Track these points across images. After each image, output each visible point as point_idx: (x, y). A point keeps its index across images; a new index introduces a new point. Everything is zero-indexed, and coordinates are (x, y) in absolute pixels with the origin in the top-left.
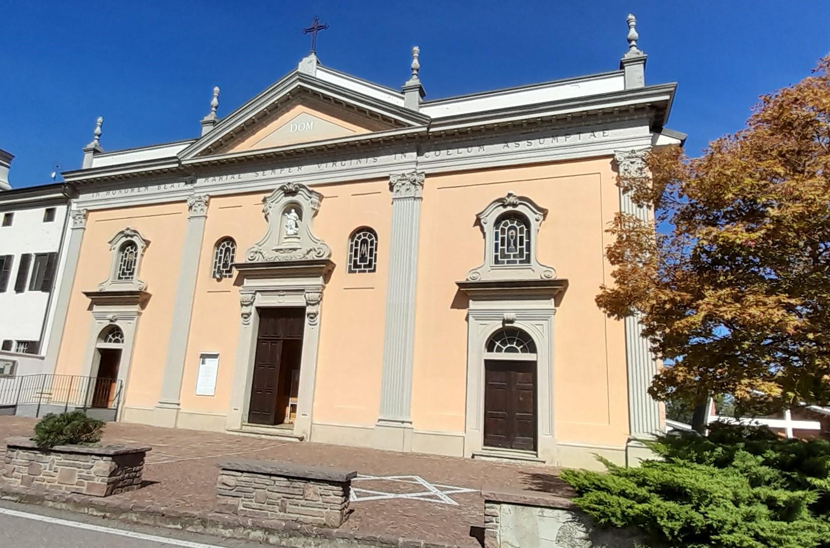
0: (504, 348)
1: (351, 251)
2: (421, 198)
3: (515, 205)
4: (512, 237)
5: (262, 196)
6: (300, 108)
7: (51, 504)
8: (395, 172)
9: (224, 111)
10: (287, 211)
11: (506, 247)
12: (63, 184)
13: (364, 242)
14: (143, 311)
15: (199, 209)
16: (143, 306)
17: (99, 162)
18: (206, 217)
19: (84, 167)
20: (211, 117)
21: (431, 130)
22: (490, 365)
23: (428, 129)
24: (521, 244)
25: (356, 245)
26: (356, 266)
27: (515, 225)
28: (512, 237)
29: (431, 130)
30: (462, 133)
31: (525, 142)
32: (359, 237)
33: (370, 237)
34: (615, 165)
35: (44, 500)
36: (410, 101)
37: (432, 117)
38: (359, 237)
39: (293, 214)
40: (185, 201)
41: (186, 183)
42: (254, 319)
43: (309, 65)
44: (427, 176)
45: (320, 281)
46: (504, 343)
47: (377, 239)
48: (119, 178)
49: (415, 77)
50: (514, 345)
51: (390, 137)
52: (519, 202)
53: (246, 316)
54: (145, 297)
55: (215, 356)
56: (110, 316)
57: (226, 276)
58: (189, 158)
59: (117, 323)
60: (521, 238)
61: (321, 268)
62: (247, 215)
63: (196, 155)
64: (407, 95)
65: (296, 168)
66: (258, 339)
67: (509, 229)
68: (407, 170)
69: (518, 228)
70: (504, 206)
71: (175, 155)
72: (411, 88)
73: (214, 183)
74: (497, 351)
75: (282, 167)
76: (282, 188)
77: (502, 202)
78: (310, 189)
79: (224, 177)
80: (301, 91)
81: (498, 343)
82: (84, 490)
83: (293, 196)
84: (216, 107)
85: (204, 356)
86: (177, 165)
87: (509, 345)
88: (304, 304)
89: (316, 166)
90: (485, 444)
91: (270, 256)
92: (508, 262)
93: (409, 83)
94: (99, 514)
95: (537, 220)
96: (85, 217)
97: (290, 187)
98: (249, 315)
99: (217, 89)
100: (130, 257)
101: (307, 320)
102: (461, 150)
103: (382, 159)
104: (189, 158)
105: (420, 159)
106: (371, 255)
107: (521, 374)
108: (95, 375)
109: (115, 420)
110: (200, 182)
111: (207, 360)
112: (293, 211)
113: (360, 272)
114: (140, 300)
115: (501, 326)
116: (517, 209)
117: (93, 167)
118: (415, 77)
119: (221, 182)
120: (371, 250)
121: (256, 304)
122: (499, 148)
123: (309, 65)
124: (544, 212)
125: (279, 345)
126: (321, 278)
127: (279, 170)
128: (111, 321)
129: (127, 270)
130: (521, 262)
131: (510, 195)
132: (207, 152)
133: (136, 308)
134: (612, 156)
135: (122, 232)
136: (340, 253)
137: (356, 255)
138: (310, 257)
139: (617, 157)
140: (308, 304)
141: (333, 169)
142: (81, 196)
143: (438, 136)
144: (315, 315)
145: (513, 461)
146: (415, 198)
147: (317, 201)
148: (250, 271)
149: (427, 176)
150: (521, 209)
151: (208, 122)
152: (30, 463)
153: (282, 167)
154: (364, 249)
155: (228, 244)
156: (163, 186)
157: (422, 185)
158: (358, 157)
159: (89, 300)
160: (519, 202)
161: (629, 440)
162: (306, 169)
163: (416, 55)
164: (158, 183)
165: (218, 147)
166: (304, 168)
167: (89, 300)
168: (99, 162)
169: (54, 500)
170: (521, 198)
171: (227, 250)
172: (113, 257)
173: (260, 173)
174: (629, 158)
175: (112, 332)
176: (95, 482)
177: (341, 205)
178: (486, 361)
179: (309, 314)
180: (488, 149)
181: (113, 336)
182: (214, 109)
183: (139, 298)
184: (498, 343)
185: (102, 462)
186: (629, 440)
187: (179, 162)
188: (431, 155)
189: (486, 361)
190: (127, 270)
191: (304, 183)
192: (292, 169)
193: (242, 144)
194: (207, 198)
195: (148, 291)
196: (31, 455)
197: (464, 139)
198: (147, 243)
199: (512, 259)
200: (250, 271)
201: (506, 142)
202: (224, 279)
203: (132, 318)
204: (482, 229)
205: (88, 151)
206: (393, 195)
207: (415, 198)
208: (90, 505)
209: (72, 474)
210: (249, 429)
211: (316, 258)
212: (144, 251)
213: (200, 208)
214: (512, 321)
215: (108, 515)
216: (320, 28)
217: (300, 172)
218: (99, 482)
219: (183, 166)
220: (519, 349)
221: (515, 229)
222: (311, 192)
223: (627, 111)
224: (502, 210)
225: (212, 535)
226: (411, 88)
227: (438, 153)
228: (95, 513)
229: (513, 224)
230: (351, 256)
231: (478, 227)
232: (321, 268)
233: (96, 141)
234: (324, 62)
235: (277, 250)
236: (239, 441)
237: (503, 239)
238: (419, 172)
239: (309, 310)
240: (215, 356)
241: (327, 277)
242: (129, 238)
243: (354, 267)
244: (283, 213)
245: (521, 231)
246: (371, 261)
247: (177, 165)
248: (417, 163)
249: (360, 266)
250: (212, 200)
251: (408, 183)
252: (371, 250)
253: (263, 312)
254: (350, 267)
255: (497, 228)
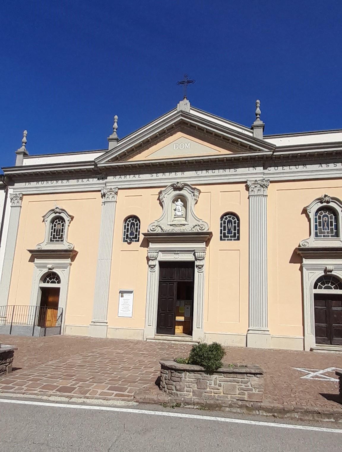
0: (50, 281)
1: (125, 229)
2: (267, 196)
3: (60, 213)
4: (326, 221)
5: (159, 190)
6: (179, 134)
7: (227, 409)
8: (251, 179)
9: (123, 134)
10: (175, 200)
11: (55, 233)
12: (3, 175)
13: (230, 221)
14: (73, 263)
15: (111, 196)
16: (73, 260)
17: (28, 162)
18: (116, 202)
19: (17, 165)
20: (114, 136)
21: (275, 154)
22: (317, 297)
23: (273, 153)
24: (332, 225)
25: (128, 225)
26: (225, 236)
27: (327, 214)
28: (326, 221)
29: (275, 154)
30: (295, 156)
31: (333, 164)
32: (130, 221)
33: (233, 219)
34: (247, 188)
35: (221, 407)
36: (258, 134)
37: (277, 145)
38: (226, 219)
39: (180, 203)
40: (100, 191)
41: (98, 179)
42: (157, 268)
43: (184, 106)
44: (271, 182)
45: (203, 245)
46: (323, 284)
47: (140, 222)
48: (47, 173)
49: (258, 119)
50: (329, 285)
51: (242, 157)
52: (331, 200)
53: (152, 267)
54: (75, 253)
55: (131, 292)
56: (50, 266)
57: (133, 241)
58: (103, 162)
59: (54, 270)
60: (331, 222)
61: (204, 237)
62: (145, 201)
63: (108, 161)
64: (255, 130)
65: (180, 173)
66: (159, 281)
67: (323, 216)
68: (259, 178)
69: (329, 216)
70: (322, 202)
71: (93, 160)
72: (257, 126)
73: (120, 180)
74: (319, 288)
75: (63, 179)
76: (172, 186)
77: (321, 200)
78: (193, 187)
79: (128, 176)
80: (182, 122)
81: (48, 279)
82: (246, 397)
83: (180, 190)
84: (117, 129)
85: (122, 293)
86: (93, 167)
87: (326, 285)
88: (194, 259)
89: (194, 172)
90: (316, 343)
91: (168, 229)
92: (324, 236)
93: (256, 123)
94: (268, 414)
95: (68, 221)
96: (21, 199)
97: (179, 185)
98: (155, 266)
99: (116, 117)
100: (59, 227)
101: (196, 269)
102: (291, 167)
103: (240, 170)
104: (103, 162)
105: (266, 171)
106: (136, 232)
107: (334, 301)
108: (39, 305)
109: (60, 334)
110: (110, 179)
111: (125, 295)
112: (179, 200)
113: (228, 240)
114: (71, 256)
115: (323, 274)
116: (61, 215)
117: (24, 165)
118: (258, 119)
119: (125, 179)
120: (137, 229)
121: (159, 259)
122: (316, 167)
123: (184, 106)
124: (72, 218)
125: (175, 285)
126: (205, 243)
127: (168, 174)
128: (50, 269)
129: (57, 235)
130: (332, 236)
131: (326, 196)
132: (116, 159)
133: (68, 261)
134: (246, 182)
135: (53, 210)
136: (214, 227)
137: (225, 230)
138: (195, 231)
139: (249, 183)
140: (196, 259)
141: (56, 185)
142: (15, 184)
143: (279, 157)
144: (202, 266)
145: (337, 352)
146: (264, 196)
147: (198, 194)
148: (150, 239)
149: (271, 182)
150: (332, 204)
151: (112, 140)
152: (198, 381)
153: (170, 172)
154: (230, 226)
155: (59, 221)
156: (80, 180)
157: (267, 187)
158: (224, 168)
159: (30, 255)
160: (331, 200)
161: (248, 330)
162: (187, 174)
163: (116, 120)
164: (78, 178)
165: (123, 156)
166: (185, 173)
167: (30, 255)
168: (28, 162)
169: (230, 406)
170: (332, 198)
171: (133, 224)
172: (46, 228)
173: (155, 175)
174: (254, 184)
175: (51, 276)
176: (254, 392)
177: (213, 198)
178: (315, 295)
179: (197, 266)
180: (309, 167)
181: (50, 279)
182: (115, 130)
183: (70, 254)
184: (48, 279)
185: (256, 378)
186: (248, 330)
187: (96, 165)
188: (272, 170)
189: (315, 295)
190: (57, 235)
191: (189, 183)
192: (177, 173)
193: (139, 155)
194: (117, 190)
195: (75, 249)
196: (198, 375)
197: (338, 157)
198: (72, 218)
199: (58, 239)
200: (150, 239)
201: (120, 175)
202: (132, 243)
203: (66, 268)
204: (308, 216)
205: (19, 153)
206: (104, 200)
207: (264, 196)
208: (260, 408)
209: (234, 387)
210: (157, 337)
211: (200, 231)
212: (70, 223)
213: (16, 201)
214: (331, 271)
215: (276, 414)
216: (189, 82)
217: (183, 176)
218: (257, 392)
219: (98, 167)
220: (56, 281)
221: (327, 216)
222: (194, 189)
223: (296, 157)
224: (320, 205)
225: (235, 413)
226: (257, 126)
227: (276, 168)
228: (265, 414)
229: (58, 222)
230: (125, 232)
231: (304, 215)
232: (204, 237)
233: (23, 147)
234: (194, 105)
235: (171, 225)
236: (151, 345)
237: (55, 229)
238: (266, 179)
239: (197, 263)
240: (131, 292)
241: (207, 242)
242: (58, 214)
243: (223, 237)
244: (173, 202)
245: (331, 218)
246: (136, 235)
247: (93, 167)
248: (264, 174)
249: (56, 238)
250: (24, 197)
251: (114, 193)
252: (137, 229)
253: (162, 264)
254: (124, 238)
255: (53, 224)
